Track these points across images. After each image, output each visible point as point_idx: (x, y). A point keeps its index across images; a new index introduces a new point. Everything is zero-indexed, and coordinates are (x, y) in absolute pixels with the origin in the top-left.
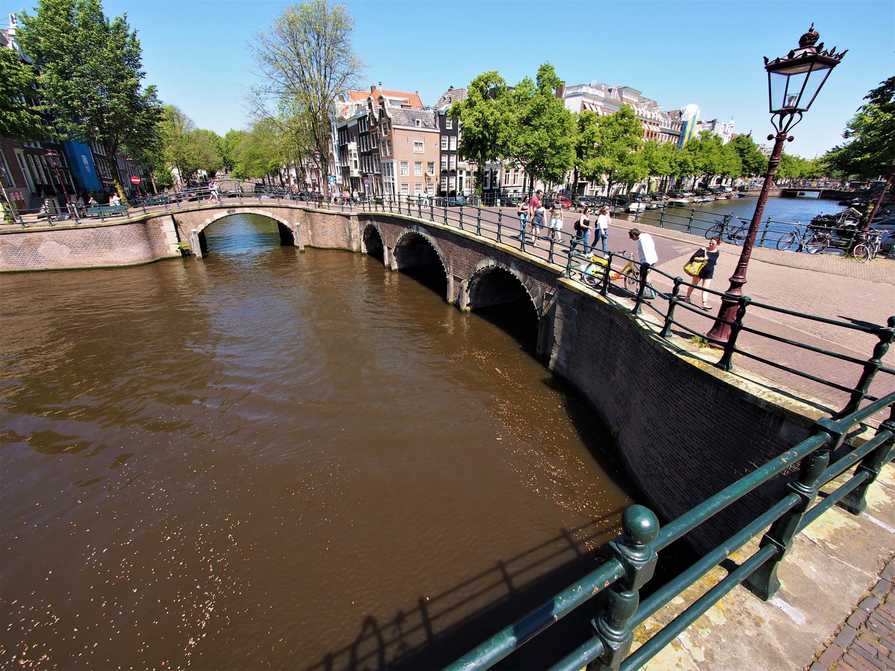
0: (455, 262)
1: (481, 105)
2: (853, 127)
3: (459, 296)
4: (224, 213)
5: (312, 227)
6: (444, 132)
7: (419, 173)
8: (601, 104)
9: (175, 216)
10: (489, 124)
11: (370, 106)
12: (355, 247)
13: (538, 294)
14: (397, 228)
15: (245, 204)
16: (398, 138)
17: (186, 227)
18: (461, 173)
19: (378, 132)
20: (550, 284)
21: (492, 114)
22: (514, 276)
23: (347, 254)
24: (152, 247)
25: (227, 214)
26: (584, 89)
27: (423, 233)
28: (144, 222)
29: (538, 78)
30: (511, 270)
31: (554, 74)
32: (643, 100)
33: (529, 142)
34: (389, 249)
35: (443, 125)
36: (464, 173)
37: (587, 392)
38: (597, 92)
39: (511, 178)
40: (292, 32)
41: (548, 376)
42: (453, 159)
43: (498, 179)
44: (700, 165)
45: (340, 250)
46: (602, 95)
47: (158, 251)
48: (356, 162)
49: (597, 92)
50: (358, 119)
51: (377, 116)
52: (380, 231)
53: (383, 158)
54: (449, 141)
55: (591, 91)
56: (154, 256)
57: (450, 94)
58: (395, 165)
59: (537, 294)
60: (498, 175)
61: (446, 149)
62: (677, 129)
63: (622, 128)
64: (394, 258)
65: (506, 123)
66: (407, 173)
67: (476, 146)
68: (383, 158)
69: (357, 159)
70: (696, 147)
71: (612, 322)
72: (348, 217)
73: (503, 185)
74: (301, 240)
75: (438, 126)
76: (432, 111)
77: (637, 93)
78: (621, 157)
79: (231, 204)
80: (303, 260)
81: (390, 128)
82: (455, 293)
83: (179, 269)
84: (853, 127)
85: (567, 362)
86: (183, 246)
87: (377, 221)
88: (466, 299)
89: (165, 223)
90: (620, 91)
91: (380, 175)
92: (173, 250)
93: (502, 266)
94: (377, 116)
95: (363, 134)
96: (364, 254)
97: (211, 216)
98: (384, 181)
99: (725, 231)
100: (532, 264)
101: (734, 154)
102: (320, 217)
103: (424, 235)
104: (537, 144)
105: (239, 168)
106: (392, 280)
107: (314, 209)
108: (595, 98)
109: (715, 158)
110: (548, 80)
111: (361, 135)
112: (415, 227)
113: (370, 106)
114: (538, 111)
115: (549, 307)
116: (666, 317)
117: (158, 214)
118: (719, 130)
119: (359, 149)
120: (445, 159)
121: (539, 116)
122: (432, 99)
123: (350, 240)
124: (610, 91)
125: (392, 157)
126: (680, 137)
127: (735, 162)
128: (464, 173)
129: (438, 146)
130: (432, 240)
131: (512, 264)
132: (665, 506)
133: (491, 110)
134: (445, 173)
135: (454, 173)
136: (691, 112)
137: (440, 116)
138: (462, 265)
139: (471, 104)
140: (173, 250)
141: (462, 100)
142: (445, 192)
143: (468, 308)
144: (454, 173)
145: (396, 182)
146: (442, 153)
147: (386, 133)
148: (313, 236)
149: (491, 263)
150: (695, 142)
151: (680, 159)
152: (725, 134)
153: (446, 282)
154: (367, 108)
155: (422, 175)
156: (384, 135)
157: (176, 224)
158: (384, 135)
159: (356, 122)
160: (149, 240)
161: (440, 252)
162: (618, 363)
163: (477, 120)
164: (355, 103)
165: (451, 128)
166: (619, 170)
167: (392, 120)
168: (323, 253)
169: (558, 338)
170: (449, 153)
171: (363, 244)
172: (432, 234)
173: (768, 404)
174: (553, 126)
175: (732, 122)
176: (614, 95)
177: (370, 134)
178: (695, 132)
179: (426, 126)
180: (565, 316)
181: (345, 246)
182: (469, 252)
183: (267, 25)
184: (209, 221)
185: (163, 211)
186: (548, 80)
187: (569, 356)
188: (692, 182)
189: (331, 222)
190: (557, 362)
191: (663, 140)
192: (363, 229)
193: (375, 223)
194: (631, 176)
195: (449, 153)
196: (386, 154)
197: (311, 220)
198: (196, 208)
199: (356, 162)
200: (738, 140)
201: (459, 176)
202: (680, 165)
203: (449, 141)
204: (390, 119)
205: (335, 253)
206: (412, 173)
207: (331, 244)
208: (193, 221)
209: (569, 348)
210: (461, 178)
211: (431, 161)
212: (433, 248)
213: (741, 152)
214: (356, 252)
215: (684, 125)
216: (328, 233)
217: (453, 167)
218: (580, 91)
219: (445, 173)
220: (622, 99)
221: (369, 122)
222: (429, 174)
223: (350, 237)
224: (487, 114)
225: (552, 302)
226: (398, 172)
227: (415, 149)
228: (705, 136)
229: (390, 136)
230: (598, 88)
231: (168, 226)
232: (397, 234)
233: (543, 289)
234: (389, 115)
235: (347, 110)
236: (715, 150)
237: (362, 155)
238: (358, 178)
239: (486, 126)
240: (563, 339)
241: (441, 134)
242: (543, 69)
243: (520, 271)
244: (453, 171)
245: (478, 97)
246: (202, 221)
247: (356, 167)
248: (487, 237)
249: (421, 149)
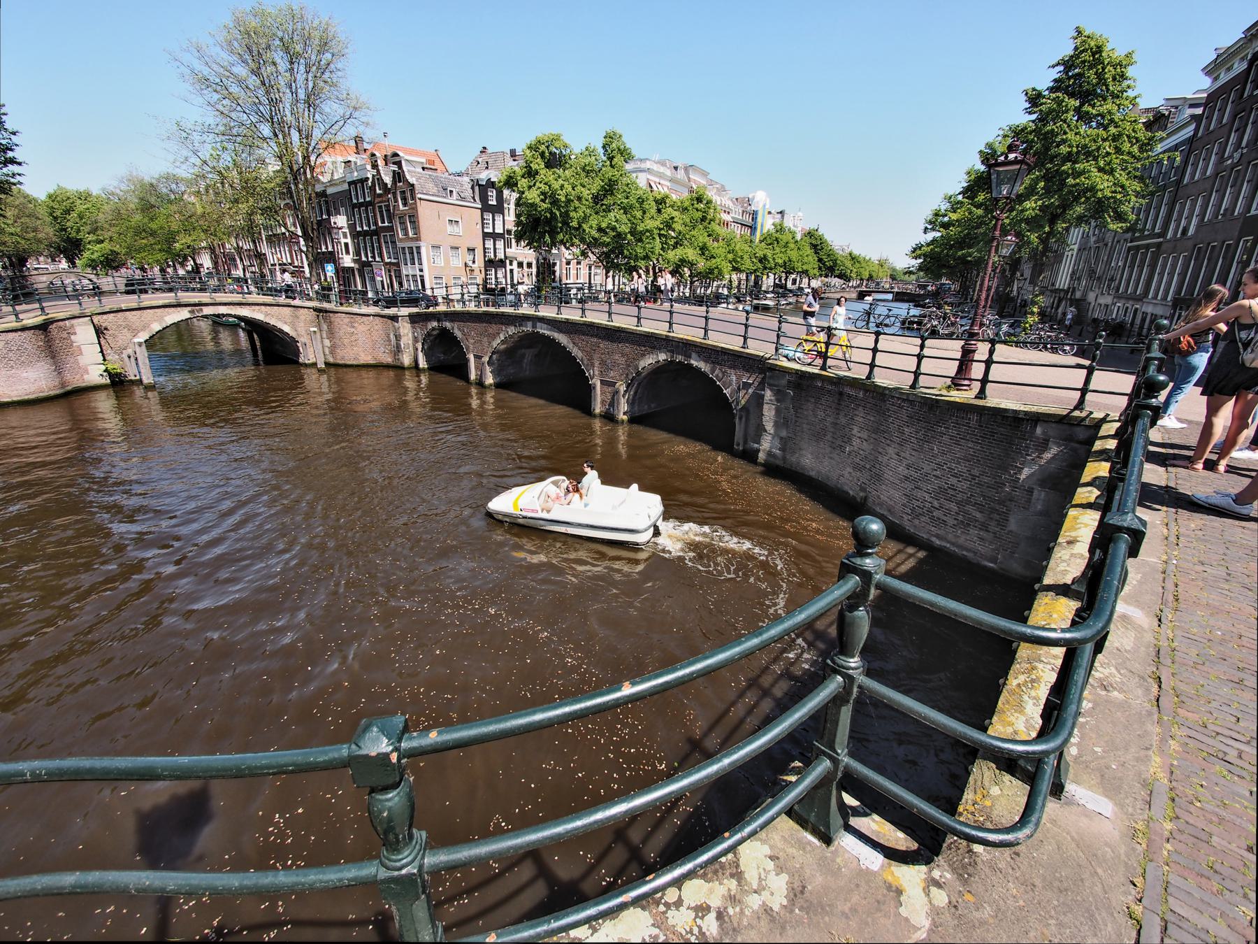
0: (603, 363)
1: (545, 174)
2: (930, 222)
3: (613, 403)
4: (184, 314)
5: (331, 334)
6: (486, 208)
7: (457, 262)
8: (668, 184)
9: (96, 319)
10: (558, 200)
11: (375, 166)
12: (407, 360)
13: (732, 384)
14: (493, 328)
15: (143, 305)
16: (426, 212)
17: (114, 336)
18: (511, 264)
19: (392, 204)
20: (747, 371)
21: (562, 187)
22: (698, 370)
23: (392, 373)
24: (59, 371)
25: (188, 316)
26: (648, 165)
27: (544, 330)
28: (44, 327)
29: (604, 147)
30: (692, 362)
31: (624, 143)
32: (711, 183)
33: (604, 225)
34: (477, 357)
35: (484, 198)
36: (515, 263)
37: (813, 474)
38: (662, 169)
39: (573, 272)
40: (254, 46)
41: (760, 469)
42: (500, 244)
43: (557, 274)
44: (780, 261)
45: (387, 367)
46: (668, 173)
47: (68, 376)
48: (346, 245)
49: (662, 169)
50: (350, 183)
51: (388, 180)
52: (458, 334)
53: (401, 240)
54: (494, 220)
55: (655, 167)
56: (63, 385)
57: (485, 157)
58: (423, 251)
59: (731, 384)
60: (557, 268)
61: (490, 230)
62: (748, 220)
63: (700, 214)
64: (488, 369)
65: (579, 199)
66: (440, 262)
67: (539, 227)
68: (401, 240)
69: (349, 240)
70: (771, 240)
71: (841, 394)
72: (394, 318)
73: (564, 281)
74: (313, 352)
75: (477, 198)
76: (466, 179)
77: (704, 174)
78: (703, 249)
79: (197, 300)
80: (318, 386)
81: (413, 198)
82: (603, 402)
83: (105, 404)
84: (930, 222)
85: (783, 449)
86: (110, 367)
87: (452, 321)
88: (623, 406)
89: (78, 330)
90: (686, 169)
91: (397, 265)
92: (95, 375)
93: (679, 358)
94: (388, 180)
95: (360, 205)
96: (424, 369)
97: (161, 319)
98: (404, 272)
99: (872, 319)
100: (724, 352)
101: (808, 251)
102: (346, 319)
103: (547, 333)
104: (614, 229)
105: (94, 251)
106: (483, 403)
107: (335, 309)
108: (661, 176)
109: (794, 255)
110: (615, 150)
111: (354, 206)
112: (530, 324)
113: (375, 166)
114: (610, 188)
115: (747, 397)
116: (915, 373)
117: (67, 315)
118: (788, 223)
119: (352, 227)
120: (489, 244)
121: (612, 194)
122: (459, 160)
123: (398, 350)
124: (676, 168)
125: (418, 239)
126: (753, 228)
127: (811, 262)
128: (515, 263)
129: (479, 226)
130: (562, 339)
131: (694, 355)
132: (937, 536)
133: (560, 182)
134: (491, 264)
135: (502, 263)
136: (761, 200)
137: (480, 186)
138: (615, 364)
139: (530, 173)
140: (95, 375)
141: (517, 167)
142: (493, 290)
143: (625, 417)
144: (502, 263)
145: (426, 274)
146: (486, 236)
147: (405, 204)
148: (333, 349)
149: (662, 357)
150: (770, 235)
151: (760, 254)
152: (798, 224)
153: (590, 389)
154: (369, 167)
155: (461, 265)
156: (401, 207)
157: (99, 332)
158: (401, 207)
159: (346, 187)
160: (53, 357)
161: (575, 352)
162: (855, 431)
163: (542, 193)
164: (340, 159)
165: (494, 203)
166: (702, 265)
167: (417, 187)
168: (351, 375)
169: (769, 427)
170: (495, 236)
171: (421, 355)
172: (561, 331)
173: (1026, 413)
174: (631, 207)
175: (800, 214)
176: (681, 174)
177: (382, 205)
178: (767, 224)
179: (463, 199)
180: (778, 400)
181: (389, 360)
182: (627, 348)
183: (208, 32)
184: (157, 327)
185: (76, 310)
186: (615, 150)
187: (785, 444)
188: (768, 282)
189: (362, 327)
190: (769, 454)
191: (738, 230)
192: (420, 334)
193: (448, 325)
194: (716, 271)
195: (495, 236)
196: (406, 234)
197: (330, 324)
198: (134, 305)
199: (346, 245)
200: (810, 234)
201: (509, 267)
202: (760, 261)
203: (494, 220)
204: (413, 185)
205: (372, 374)
206: (447, 261)
207: (366, 358)
208: (129, 328)
209: (784, 433)
210: (511, 271)
211: (471, 246)
212: (564, 348)
213: (814, 246)
214: (409, 368)
215: (754, 215)
216: (360, 342)
217: (501, 255)
218: (643, 166)
219: (491, 264)
220: (689, 179)
221: (373, 188)
222: (470, 263)
223: (398, 346)
224: (556, 185)
225: (750, 391)
226: (429, 261)
227: (449, 229)
228: (780, 229)
229: (415, 208)
230: (663, 164)
231: (84, 334)
232: (494, 336)
233: (739, 378)
234: (411, 180)
235: (332, 169)
236: (792, 246)
237: (356, 235)
238: (352, 269)
239: (555, 202)
240: (776, 425)
241: (483, 210)
242: (610, 137)
243: (706, 361)
244: (501, 261)
245: (538, 165)
246: (144, 328)
247: (348, 252)
248: (660, 329)
249: (458, 230)
